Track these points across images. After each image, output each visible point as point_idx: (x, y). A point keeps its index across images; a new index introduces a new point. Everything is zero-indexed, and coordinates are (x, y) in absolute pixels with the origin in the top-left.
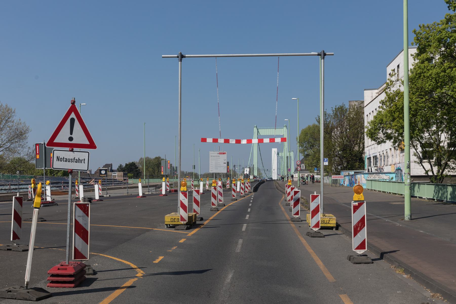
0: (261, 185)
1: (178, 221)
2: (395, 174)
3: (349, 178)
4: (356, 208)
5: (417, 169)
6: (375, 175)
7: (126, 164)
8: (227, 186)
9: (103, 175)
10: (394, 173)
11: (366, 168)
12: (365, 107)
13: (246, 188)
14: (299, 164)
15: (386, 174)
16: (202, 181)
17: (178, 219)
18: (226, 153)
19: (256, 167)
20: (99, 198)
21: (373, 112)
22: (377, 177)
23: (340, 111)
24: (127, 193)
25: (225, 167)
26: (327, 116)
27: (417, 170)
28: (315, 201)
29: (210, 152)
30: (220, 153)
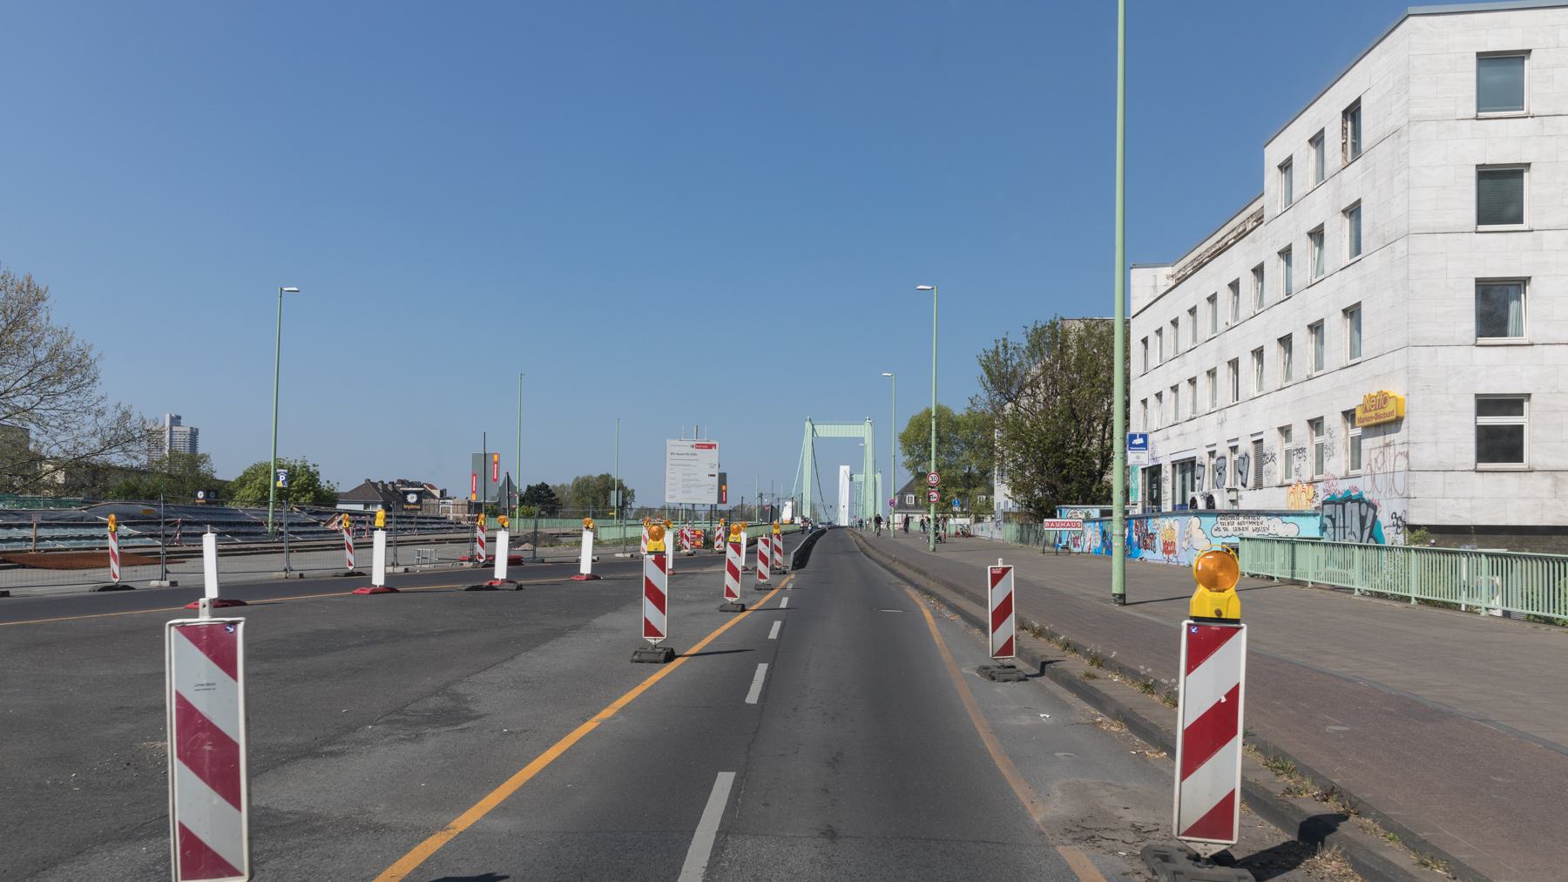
0: (818, 542)
2: (1318, 518)
3: (1101, 527)
4: (996, 579)
5: (1456, 498)
6: (1241, 519)
7: (529, 486)
8: (716, 544)
9: (412, 507)
10: (1315, 515)
11: (1137, 498)
12: (1133, 317)
13: (769, 556)
14: (933, 482)
15: (1285, 519)
16: (503, 526)
18: (715, 445)
19: (807, 498)
21: (1259, 271)
22: (1250, 529)
23: (1048, 339)
24: (286, 570)
25: (711, 487)
26: (1009, 352)
27: (1453, 502)
29: (669, 442)
30: (699, 445)
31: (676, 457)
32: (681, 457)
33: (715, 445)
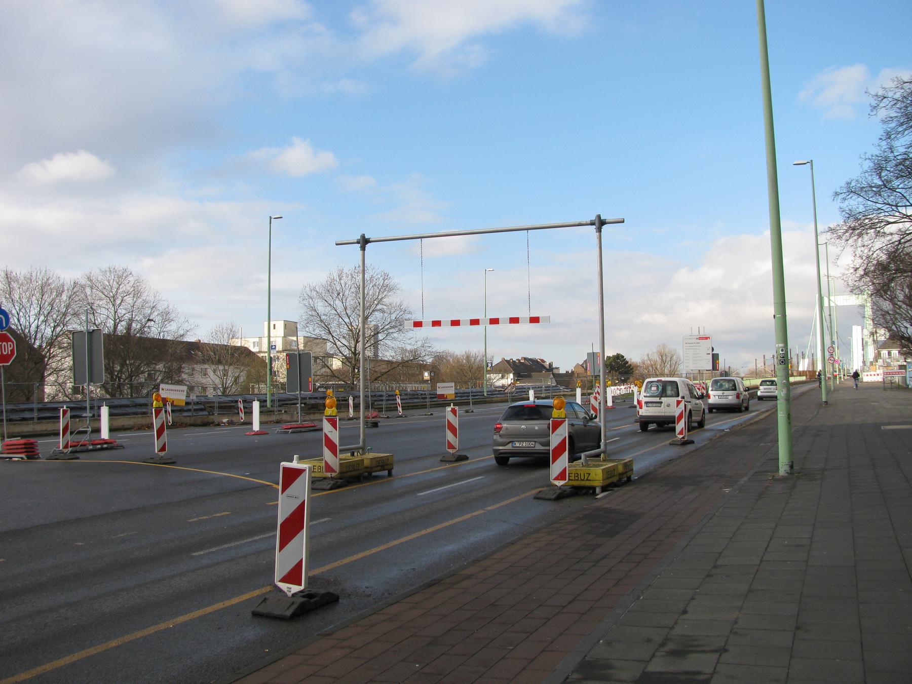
1: (319, 470)
17: (319, 468)
20: (260, 428)
28: (558, 431)
30: (701, 338)
31: (688, 345)
32: (692, 345)
33: (709, 338)
